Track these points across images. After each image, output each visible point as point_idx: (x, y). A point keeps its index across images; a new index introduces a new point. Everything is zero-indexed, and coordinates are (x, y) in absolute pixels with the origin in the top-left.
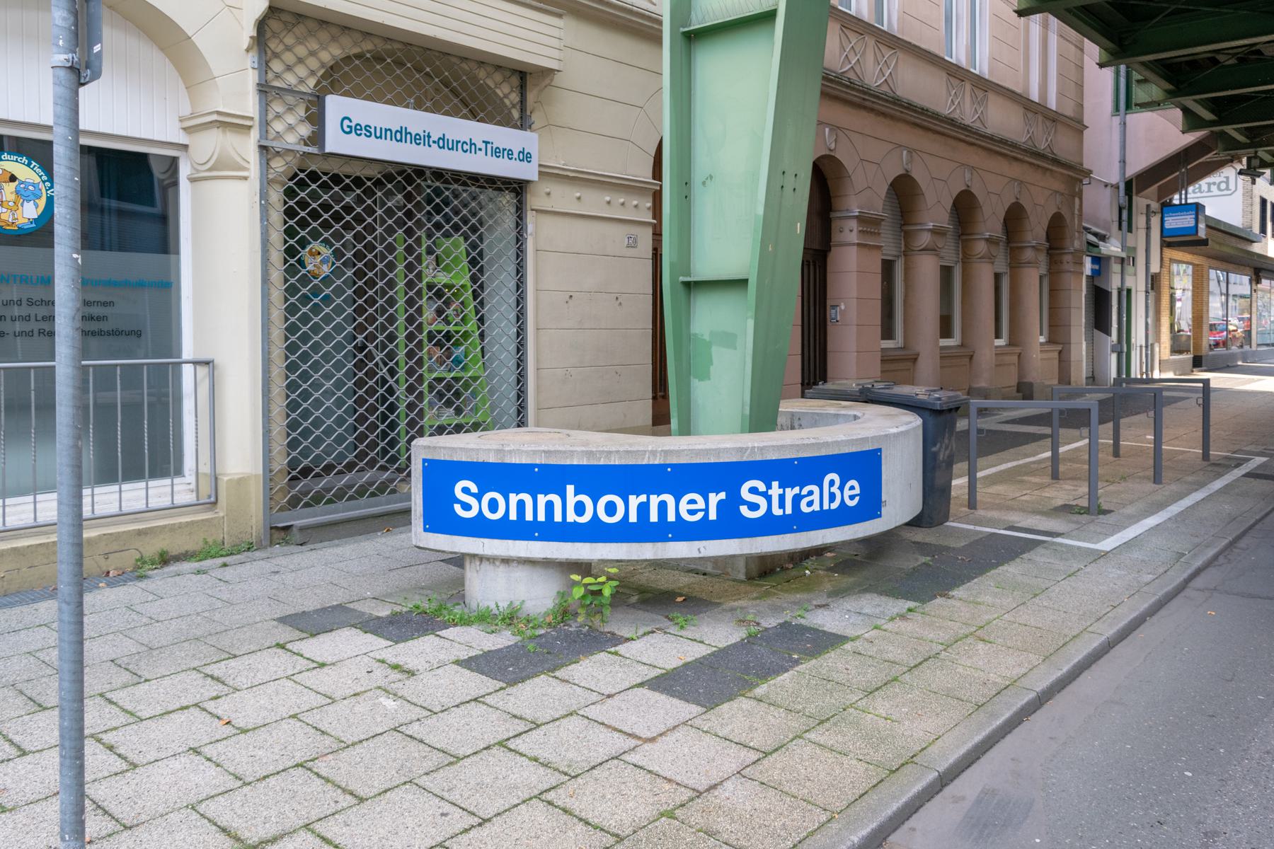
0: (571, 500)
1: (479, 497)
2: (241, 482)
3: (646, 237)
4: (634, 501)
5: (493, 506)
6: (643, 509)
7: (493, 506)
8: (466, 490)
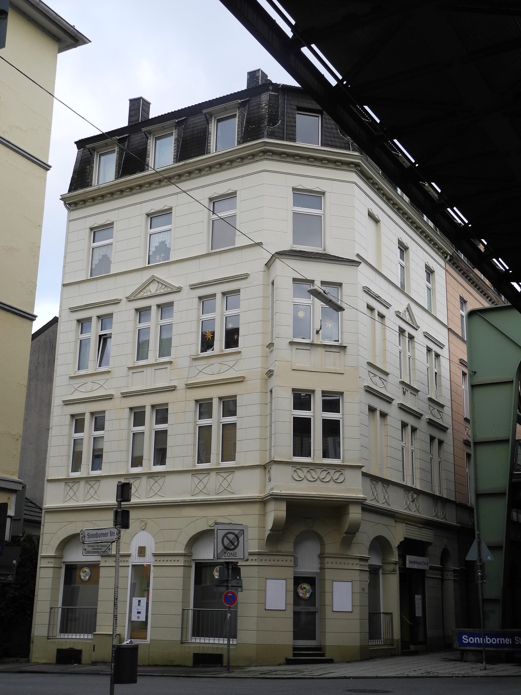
0: (487, 639)
1: (468, 638)
2: (398, 640)
3: (402, 474)
4: (498, 639)
5: (471, 640)
6: (500, 641)
7: (471, 640)
8: (465, 637)
